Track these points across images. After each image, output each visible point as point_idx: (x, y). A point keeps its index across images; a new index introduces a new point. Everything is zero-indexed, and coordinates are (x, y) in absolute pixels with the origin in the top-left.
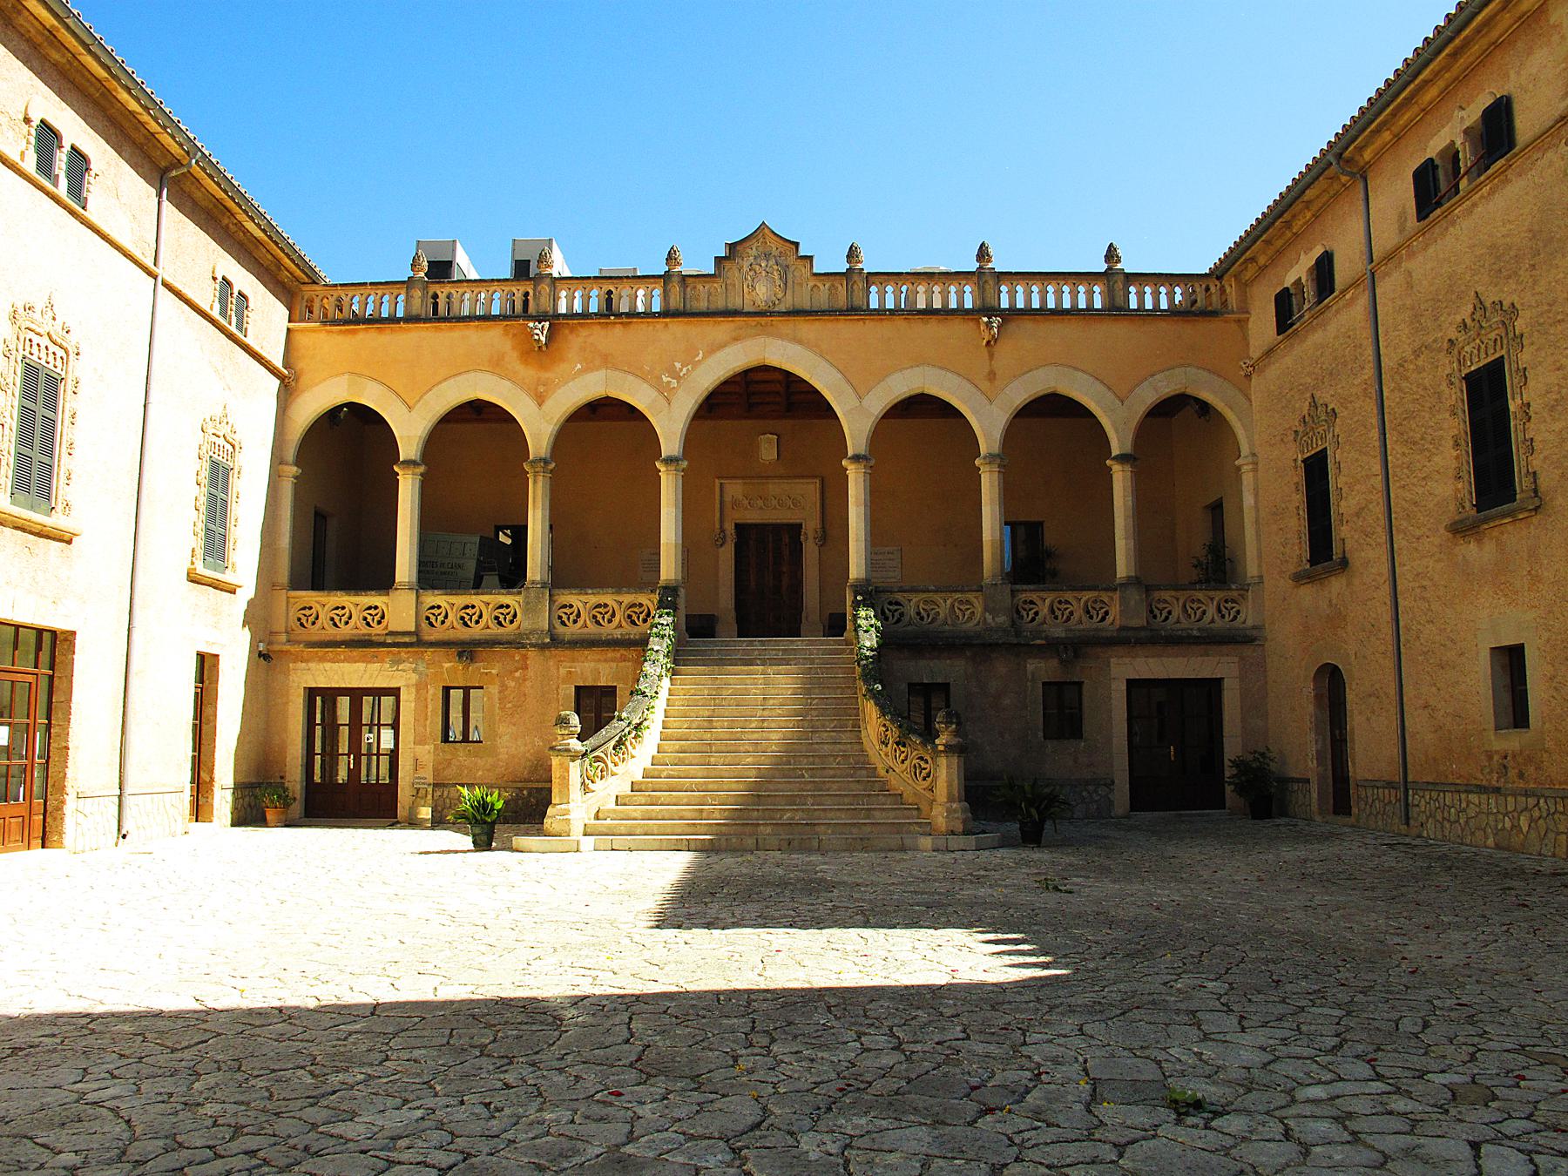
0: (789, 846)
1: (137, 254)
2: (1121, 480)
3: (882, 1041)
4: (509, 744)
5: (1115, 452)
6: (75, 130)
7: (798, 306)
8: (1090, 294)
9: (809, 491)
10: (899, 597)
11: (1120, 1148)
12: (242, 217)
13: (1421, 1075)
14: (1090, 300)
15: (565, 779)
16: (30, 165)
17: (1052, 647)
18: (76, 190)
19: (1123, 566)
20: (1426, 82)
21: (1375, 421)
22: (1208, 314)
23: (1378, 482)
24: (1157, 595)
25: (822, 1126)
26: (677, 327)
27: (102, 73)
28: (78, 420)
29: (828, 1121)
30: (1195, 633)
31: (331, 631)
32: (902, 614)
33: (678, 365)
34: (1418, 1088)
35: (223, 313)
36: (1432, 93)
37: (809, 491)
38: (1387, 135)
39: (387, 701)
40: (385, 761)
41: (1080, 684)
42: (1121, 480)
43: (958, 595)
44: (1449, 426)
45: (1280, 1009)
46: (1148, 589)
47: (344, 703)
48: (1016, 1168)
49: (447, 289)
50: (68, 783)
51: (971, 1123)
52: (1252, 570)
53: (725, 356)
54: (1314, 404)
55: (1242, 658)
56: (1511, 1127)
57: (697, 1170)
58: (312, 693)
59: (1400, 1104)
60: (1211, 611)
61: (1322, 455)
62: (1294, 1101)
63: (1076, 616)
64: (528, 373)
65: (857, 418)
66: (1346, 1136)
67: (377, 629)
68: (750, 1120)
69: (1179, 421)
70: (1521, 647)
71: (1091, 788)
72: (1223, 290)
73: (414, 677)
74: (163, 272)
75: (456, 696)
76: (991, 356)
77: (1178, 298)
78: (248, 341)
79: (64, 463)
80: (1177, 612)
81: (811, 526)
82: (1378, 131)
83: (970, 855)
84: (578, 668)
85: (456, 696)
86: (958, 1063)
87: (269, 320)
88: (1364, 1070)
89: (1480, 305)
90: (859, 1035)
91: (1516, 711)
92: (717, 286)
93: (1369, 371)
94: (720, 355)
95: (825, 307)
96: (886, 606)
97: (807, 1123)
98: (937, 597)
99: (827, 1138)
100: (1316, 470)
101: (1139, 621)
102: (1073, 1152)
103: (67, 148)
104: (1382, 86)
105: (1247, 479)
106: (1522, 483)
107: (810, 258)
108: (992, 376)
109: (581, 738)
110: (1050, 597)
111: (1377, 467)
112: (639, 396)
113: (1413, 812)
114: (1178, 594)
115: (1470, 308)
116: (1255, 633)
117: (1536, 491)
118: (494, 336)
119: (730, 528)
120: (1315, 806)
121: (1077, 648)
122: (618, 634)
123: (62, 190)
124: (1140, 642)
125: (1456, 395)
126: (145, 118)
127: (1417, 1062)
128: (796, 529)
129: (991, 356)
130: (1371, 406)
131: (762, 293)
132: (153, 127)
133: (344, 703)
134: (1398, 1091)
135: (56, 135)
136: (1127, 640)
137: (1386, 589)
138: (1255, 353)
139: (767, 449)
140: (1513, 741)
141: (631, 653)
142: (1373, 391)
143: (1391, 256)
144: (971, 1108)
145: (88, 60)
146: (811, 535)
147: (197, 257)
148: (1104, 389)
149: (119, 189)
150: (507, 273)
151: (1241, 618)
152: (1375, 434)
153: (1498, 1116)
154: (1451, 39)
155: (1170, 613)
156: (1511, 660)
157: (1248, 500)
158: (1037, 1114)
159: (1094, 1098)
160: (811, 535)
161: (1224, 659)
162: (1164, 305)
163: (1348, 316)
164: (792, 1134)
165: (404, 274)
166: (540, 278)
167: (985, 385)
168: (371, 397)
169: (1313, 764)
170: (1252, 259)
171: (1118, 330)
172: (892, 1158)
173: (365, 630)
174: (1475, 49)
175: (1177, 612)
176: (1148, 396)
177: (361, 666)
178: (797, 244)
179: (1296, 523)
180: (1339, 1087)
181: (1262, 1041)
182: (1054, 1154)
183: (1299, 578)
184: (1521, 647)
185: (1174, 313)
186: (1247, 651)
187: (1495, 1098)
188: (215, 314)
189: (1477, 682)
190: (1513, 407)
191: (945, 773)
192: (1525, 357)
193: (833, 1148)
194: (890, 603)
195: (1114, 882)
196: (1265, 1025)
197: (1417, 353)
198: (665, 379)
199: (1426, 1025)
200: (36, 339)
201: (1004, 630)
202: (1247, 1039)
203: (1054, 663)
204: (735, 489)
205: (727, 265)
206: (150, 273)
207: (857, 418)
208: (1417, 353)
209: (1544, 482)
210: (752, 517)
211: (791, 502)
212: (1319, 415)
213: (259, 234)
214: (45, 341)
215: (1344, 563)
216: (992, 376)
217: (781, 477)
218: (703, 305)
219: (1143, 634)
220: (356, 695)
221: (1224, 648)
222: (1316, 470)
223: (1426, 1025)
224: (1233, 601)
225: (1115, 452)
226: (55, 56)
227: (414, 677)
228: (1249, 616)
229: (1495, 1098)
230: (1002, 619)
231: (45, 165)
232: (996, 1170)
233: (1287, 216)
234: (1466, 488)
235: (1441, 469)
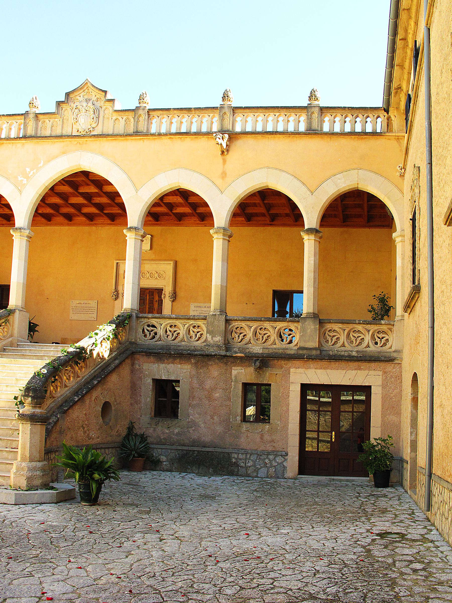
7: (105, 132)
17: (249, 358)
24: (329, 326)
26: (29, 145)
30: (354, 354)
32: (156, 334)
33: (28, 170)
43: (192, 322)
46: (321, 323)
53: (55, 165)
55: (385, 372)
60: (367, 338)
63: (272, 339)
71: (271, 457)
76: (224, 161)
80: (343, 338)
92: (57, 120)
95: (122, 132)
96: (146, 327)
98: (177, 322)
101: (314, 344)
107: (112, 100)
108: (224, 175)
114: (344, 326)
116: (395, 355)
124: (311, 358)
128: (160, 291)
129: (224, 161)
131: (84, 123)
136: (304, 356)
146: (167, 295)
148: (300, 184)
151: (388, 346)
155: (338, 338)
160: (167, 295)
161: (372, 372)
167: (219, 182)
171: (314, 143)
175: (343, 338)
178: (105, 92)
186: (389, 367)
194: (148, 326)
198: (20, 179)
201: (218, 346)
203: (251, 369)
205: (64, 106)
216: (224, 175)
217: (152, 260)
218: (48, 133)
219: (314, 352)
221: (373, 365)
224: (384, 332)
225: (306, 227)
230: (218, 339)
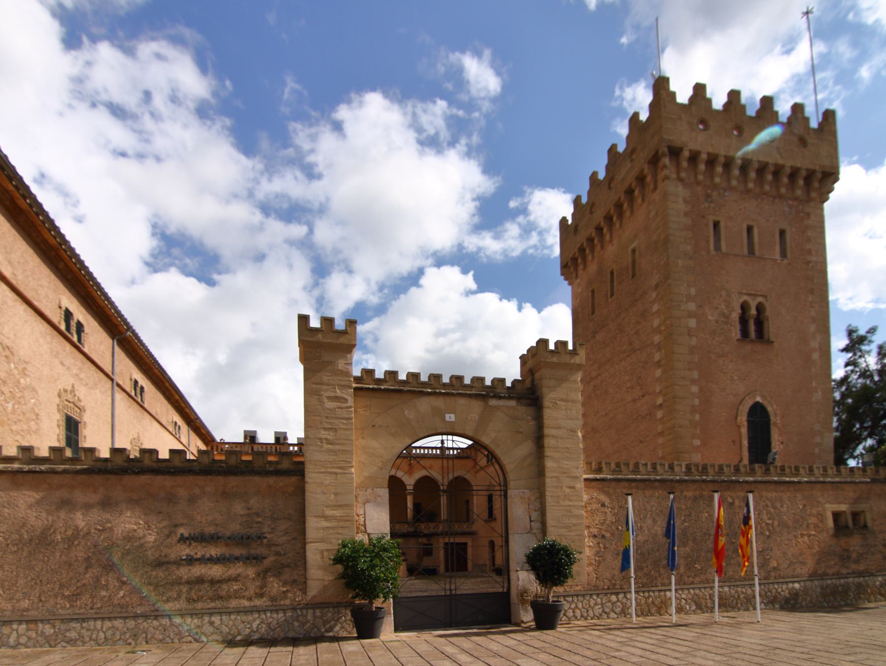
2: (444, 500)
19: (444, 514)
22: (467, 458)
42: (444, 500)
123: (75, 339)
156: (759, 419)
157: (475, 501)
228: (474, 528)
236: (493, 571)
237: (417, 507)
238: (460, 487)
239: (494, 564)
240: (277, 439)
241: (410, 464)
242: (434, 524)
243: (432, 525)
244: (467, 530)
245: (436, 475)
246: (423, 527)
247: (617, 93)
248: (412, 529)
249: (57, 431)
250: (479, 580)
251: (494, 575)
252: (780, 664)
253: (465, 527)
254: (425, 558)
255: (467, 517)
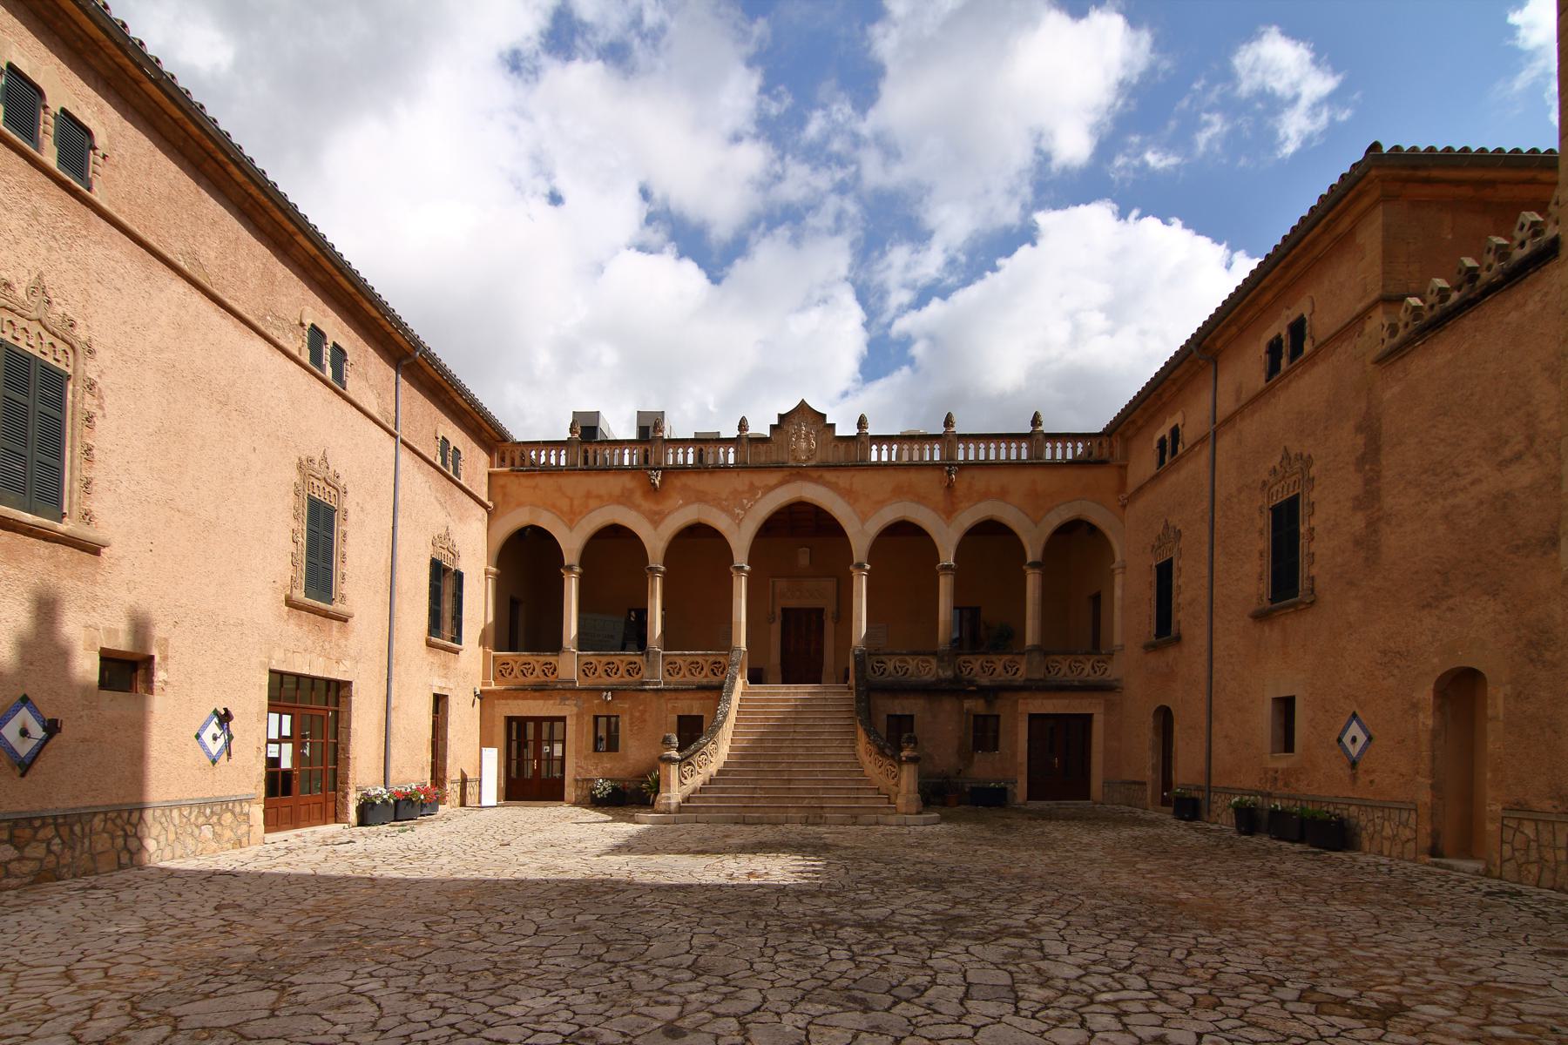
0: (807, 822)
1: (383, 421)
2: (1033, 581)
3: (844, 954)
4: (635, 752)
5: (1029, 560)
6: (337, 330)
8: (1019, 449)
9: (829, 585)
10: (884, 658)
11: (976, 1029)
12: (454, 394)
13: (1177, 988)
14: (1019, 454)
15: (668, 777)
16: (306, 358)
18: (338, 375)
19: (1031, 635)
20: (1264, 289)
21: (1207, 539)
22: (1101, 463)
23: (1206, 581)
25: (797, 1009)
27: (351, 290)
28: (349, 539)
29: (801, 1007)
31: (522, 679)
34: (1173, 996)
35: (444, 462)
36: (1269, 296)
37: (829, 585)
38: (1234, 329)
39: (558, 725)
40: (557, 765)
41: (998, 717)
42: (1033, 581)
44: (1260, 543)
45: (1098, 940)
46: (1046, 654)
47: (531, 726)
48: (909, 1040)
49: (593, 447)
50: (351, 781)
51: (888, 1010)
52: (1117, 640)
54: (1166, 526)
56: (1225, 1025)
57: (717, 1037)
58: (509, 720)
59: (1159, 1007)
61: (1169, 563)
62: (1092, 1002)
64: (647, 505)
65: (861, 534)
66: (1120, 1027)
67: (551, 678)
68: (754, 1005)
69: (1077, 540)
70: (1293, 698)
72: (1111, 446)
73: (575, 710)
74: (402, 434)
75: (602, 721)
77: (1079, 451)
78: (462, 482)
79: (338, 568)
81: (830, 609)
82: (1228, 326)
83: (920, 829)
84: (679, 704)
85: (602, 721)
86: (886, 970)
87: (476, 465)
88: (1139, 983)
89: (1286, 455)
90: (830, 950)
91: (1287, 742)
93: (1206, 504)
94: (772, 494)
97: (788, 1007)
99: (799, 1017)
100: (1165, 573)
102: (947, 1031)
103: (330, 345)
104: (620, 425)
105: (1118, 579)
106: (1303, 584)
109: (679, 750)
110: (981, 659)
111: (1206, 572)
112: (721, 522)
113: (1213, 807)
115: (1278, 458)
117: (1312, 590)
118: (626, 481)
119: (778, 611)
120: (1149, 800)
121: (991, 693)
122: (705, 681)
123: (329, 373)
125: (1264, 522)
126: (383, 322)
127: (1177, 979)
128: (821, 611)
130: (1205, 529)
132: (389, 329)
133: (531, 726)
134: (1160, 998)
135: (323, 335)
137: (1205, 656)
138: (1130, 489)
139: (804, 558)
140: (1283, 762)
141: (713, 695)
142: (1207, 518)
143: (1230, 420)
144: (889, 999)
145: (341, 280)
147: (430, 424)
149: (370, 374)
150: (633, 436)
152: (1206, 548)
153: (1220, 1016)
154: (1285, 256)
156: (1286, 706)
157: (1118, 592)
158: (929, 1005)
159: (967, 995)
162: (1069, 456)
163: (1198, 465)
164: (778, 1014)
165: (565, 435)
166: (655, 439)
168: (546, 521)
169: (1149, 773)
170: (1134, 422)
171: (1038, 475)
172: (835, 1032)
173: (543, 678)
174: (1303, 262)
176: (1055, 520)
177: (541, 702)
179: (1149, 610)
180: (1124, 994)
181: (1080, 961)
182: (932, 1032)
183: (1150, 648)
184: (1293, 698)
185: (1075, 463)
187: (1221, 1004)
188: (438, 463)
189: (1264, 719)
190: (1302, 530)
191: (908, 778)
192: (1314, 496)
193: (800, 1024)
195: (920, 889)
196: (1084, 951)
197: (1240, 491)
199: (1189, 953)
200: (316, 483)
202: (1070, 959)
204: (782, 584)
206: (392, 434)
207: (861, 534)
208: (1240, 491)
209: (1319, 584)
210: (793, 603)
211: (813, 594)
212: (1171, 535)
213: (466, 406)
214: (322, 484)
215: (1178, 639)
220: (538, 720)
222: (1165, 573)
223: (1189, 953)
225: (1029, 560)
226: (319, 276)
227: (575, 710)
228: (1114, 671)
229: (1221, 1004)
231: (316, 357)
232: (897, 1042)
233: (1159, 390)
234: (1265, 588)
235: (1249, 575)
236: (1165, 802)
237: (966, 613)
238: (1077, 540)
239: (1167, 783)
240: (643, 430)
241: (950, 487)
242: (1006, 658)
243: (999, 662)
244: (1095, 678)
245: (1010, 515)
246: (982, 669)
247: (1133, 103)
248: (949, 674)
249: (292, 547)
250: (1126, 833)
251: (1167, 814)
252: (270, 1042)
253: (1087, 670)
254: (978, 756)
255: (1096, 644)
